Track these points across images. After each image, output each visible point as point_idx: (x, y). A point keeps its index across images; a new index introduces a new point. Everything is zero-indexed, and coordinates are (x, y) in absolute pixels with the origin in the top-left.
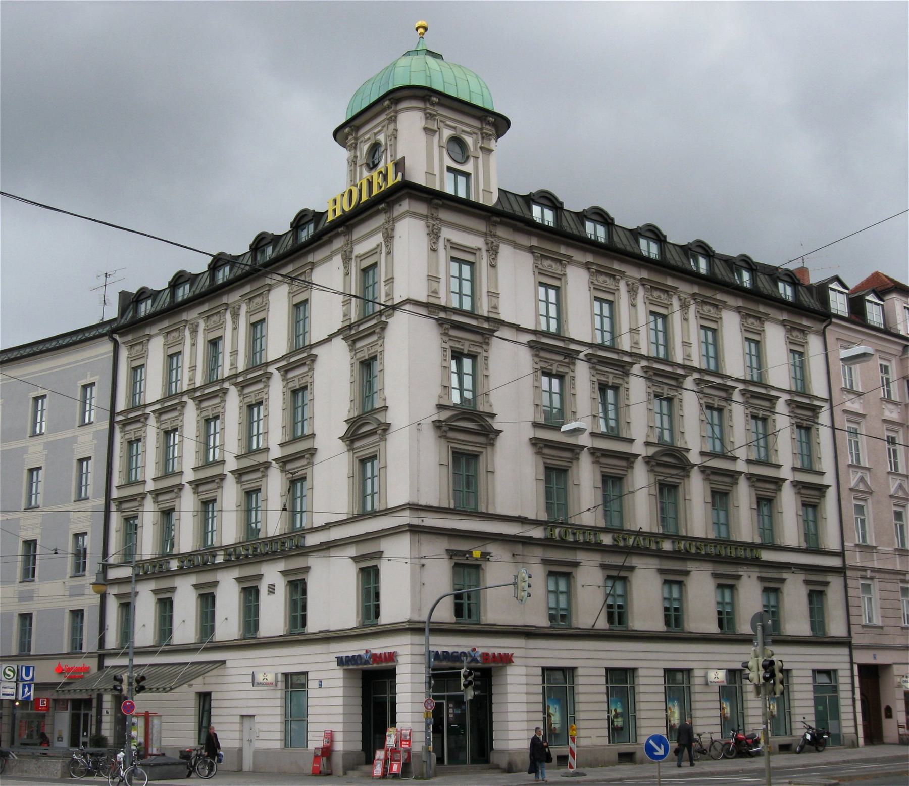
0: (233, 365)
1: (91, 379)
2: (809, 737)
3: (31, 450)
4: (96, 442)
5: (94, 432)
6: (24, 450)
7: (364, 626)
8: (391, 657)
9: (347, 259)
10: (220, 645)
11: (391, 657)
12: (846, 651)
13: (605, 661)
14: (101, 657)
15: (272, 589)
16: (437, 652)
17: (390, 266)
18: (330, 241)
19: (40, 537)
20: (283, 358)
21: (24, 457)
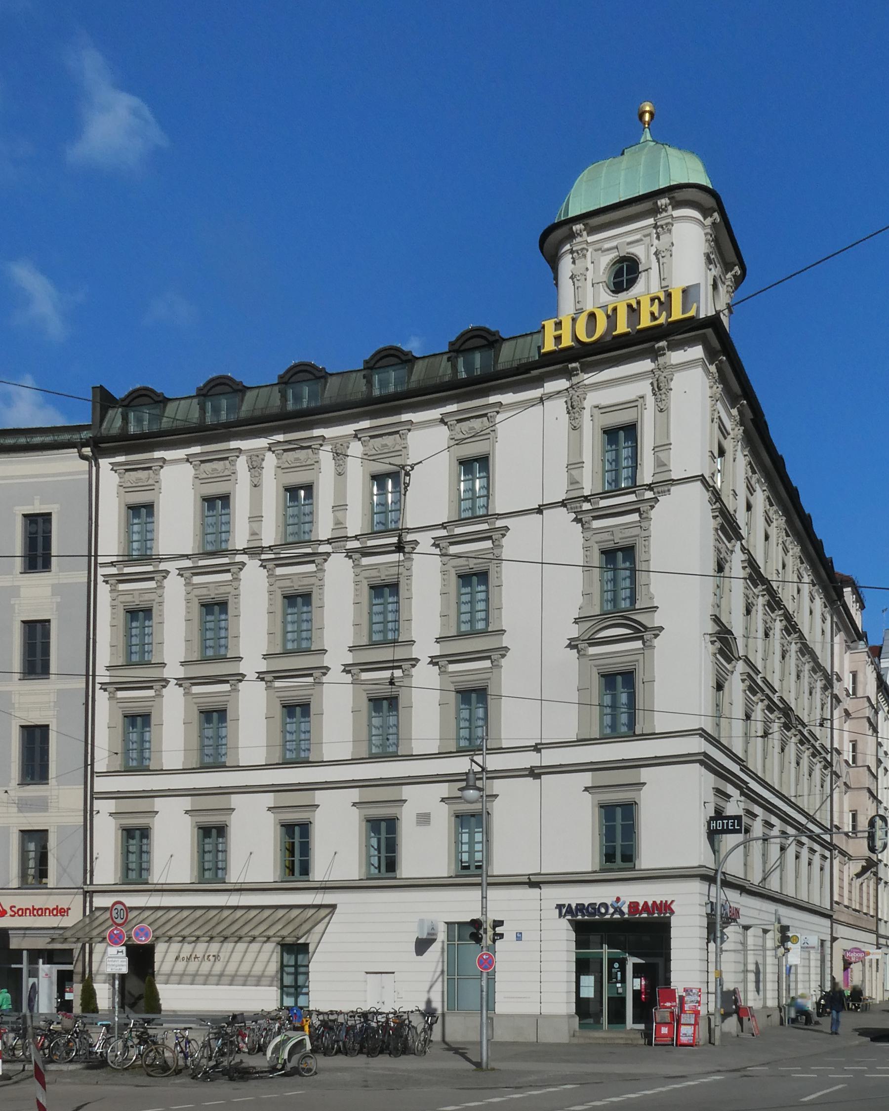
0: (339, 524)
1: (43, 507)
2: (823, 1002)
3: (23, 591)
4: (59, 600)
5: (53, 585)
6: (15, 591)
7: (602, 870)
8: (666, 907)
9: (573, 409)
10: (159, 887)
11: (666, 907)
12: (827, 922)
13: (752, 919)
14: (88, 895)
15: (424, 819)
16: (569, 905)
17: (663, 428)
18: (538, 382)
19: (54, 720)
20: (443, 526)
21: (12, 602)
